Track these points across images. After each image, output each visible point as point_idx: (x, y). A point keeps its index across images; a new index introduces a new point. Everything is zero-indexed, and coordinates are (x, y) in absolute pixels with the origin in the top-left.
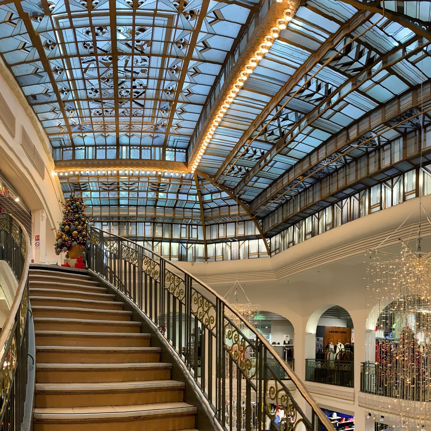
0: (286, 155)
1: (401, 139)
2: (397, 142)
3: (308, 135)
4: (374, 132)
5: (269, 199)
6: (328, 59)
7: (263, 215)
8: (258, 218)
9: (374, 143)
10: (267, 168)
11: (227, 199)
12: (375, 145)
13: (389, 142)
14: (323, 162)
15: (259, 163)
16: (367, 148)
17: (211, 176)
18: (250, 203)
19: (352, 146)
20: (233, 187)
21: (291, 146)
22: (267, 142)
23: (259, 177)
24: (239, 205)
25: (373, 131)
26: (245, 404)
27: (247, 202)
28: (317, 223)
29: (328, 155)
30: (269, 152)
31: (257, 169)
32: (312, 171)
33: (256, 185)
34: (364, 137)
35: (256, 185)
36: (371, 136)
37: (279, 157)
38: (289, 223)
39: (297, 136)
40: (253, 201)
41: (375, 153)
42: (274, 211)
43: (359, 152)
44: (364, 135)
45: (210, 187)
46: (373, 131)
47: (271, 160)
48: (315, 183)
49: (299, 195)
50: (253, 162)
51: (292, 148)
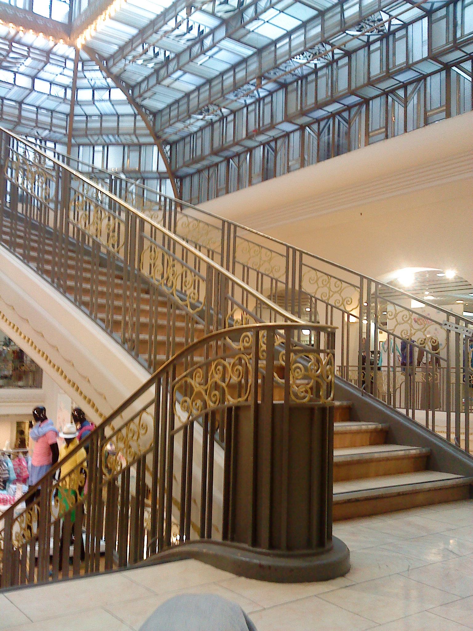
0: (239, 41)
1: (425, 20)
2: (417, 25)
3: (281, 11)
4: (384, 12)
5: (194, 113)
6: (188, 40)
7: (174, 138)
8: (167, 142)
9: (381, 28)
10: (202, 59)
11: (120, 103)
12: (382, 31)
13: (405, 26)
14: (298, 57)
15: (190, 48)
16: (369, 36)
17: (102, 58)
18: (155, 114)
19: (347, 34)
20: (133, 83)
21: (250, 27)
22: (213, 14)
23: (185, 73)
24: (135, 115)
25: (384, 9)
26: (266, 337)
27: (151, 113)
28: (273, 158)
29: (308, 46)
30: (213, 31)
31: (185, 58)
32: (277, 70)
33: (176, 85)
34: (368, 20)
35: (176, 85)
36: (380, 17)
37: (228, 44)
38: (221, 156)
39: (265, 11)
40: (160, 111)
41: (382, 44)
42: (196, 133)
43: (356, 43)
44: (370, 17)
45: (96, 76)
46: (384, 9)
47: (214, 46)
48: (276, 91)
49: (245, 109)
50: (183, 44)
51: (251, 30)
